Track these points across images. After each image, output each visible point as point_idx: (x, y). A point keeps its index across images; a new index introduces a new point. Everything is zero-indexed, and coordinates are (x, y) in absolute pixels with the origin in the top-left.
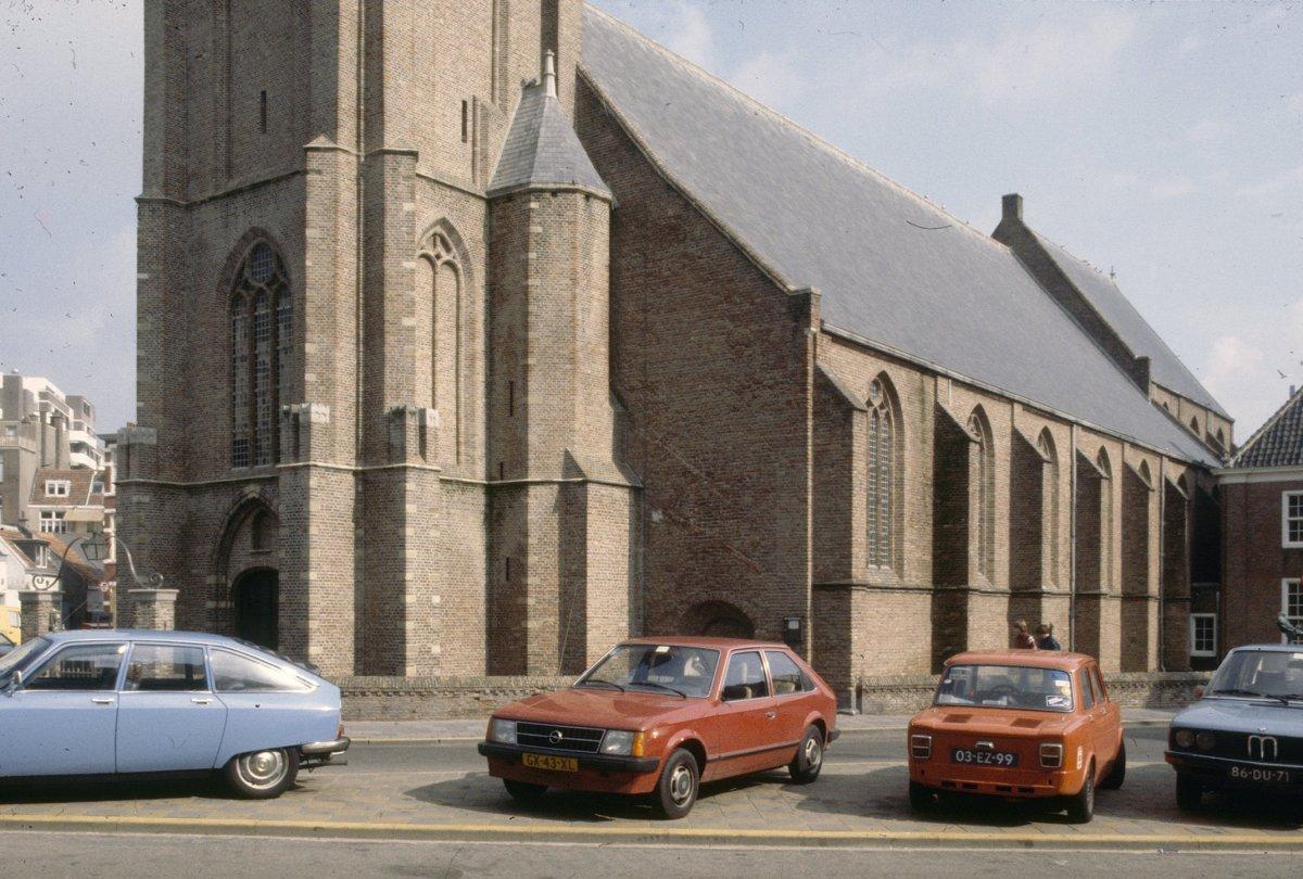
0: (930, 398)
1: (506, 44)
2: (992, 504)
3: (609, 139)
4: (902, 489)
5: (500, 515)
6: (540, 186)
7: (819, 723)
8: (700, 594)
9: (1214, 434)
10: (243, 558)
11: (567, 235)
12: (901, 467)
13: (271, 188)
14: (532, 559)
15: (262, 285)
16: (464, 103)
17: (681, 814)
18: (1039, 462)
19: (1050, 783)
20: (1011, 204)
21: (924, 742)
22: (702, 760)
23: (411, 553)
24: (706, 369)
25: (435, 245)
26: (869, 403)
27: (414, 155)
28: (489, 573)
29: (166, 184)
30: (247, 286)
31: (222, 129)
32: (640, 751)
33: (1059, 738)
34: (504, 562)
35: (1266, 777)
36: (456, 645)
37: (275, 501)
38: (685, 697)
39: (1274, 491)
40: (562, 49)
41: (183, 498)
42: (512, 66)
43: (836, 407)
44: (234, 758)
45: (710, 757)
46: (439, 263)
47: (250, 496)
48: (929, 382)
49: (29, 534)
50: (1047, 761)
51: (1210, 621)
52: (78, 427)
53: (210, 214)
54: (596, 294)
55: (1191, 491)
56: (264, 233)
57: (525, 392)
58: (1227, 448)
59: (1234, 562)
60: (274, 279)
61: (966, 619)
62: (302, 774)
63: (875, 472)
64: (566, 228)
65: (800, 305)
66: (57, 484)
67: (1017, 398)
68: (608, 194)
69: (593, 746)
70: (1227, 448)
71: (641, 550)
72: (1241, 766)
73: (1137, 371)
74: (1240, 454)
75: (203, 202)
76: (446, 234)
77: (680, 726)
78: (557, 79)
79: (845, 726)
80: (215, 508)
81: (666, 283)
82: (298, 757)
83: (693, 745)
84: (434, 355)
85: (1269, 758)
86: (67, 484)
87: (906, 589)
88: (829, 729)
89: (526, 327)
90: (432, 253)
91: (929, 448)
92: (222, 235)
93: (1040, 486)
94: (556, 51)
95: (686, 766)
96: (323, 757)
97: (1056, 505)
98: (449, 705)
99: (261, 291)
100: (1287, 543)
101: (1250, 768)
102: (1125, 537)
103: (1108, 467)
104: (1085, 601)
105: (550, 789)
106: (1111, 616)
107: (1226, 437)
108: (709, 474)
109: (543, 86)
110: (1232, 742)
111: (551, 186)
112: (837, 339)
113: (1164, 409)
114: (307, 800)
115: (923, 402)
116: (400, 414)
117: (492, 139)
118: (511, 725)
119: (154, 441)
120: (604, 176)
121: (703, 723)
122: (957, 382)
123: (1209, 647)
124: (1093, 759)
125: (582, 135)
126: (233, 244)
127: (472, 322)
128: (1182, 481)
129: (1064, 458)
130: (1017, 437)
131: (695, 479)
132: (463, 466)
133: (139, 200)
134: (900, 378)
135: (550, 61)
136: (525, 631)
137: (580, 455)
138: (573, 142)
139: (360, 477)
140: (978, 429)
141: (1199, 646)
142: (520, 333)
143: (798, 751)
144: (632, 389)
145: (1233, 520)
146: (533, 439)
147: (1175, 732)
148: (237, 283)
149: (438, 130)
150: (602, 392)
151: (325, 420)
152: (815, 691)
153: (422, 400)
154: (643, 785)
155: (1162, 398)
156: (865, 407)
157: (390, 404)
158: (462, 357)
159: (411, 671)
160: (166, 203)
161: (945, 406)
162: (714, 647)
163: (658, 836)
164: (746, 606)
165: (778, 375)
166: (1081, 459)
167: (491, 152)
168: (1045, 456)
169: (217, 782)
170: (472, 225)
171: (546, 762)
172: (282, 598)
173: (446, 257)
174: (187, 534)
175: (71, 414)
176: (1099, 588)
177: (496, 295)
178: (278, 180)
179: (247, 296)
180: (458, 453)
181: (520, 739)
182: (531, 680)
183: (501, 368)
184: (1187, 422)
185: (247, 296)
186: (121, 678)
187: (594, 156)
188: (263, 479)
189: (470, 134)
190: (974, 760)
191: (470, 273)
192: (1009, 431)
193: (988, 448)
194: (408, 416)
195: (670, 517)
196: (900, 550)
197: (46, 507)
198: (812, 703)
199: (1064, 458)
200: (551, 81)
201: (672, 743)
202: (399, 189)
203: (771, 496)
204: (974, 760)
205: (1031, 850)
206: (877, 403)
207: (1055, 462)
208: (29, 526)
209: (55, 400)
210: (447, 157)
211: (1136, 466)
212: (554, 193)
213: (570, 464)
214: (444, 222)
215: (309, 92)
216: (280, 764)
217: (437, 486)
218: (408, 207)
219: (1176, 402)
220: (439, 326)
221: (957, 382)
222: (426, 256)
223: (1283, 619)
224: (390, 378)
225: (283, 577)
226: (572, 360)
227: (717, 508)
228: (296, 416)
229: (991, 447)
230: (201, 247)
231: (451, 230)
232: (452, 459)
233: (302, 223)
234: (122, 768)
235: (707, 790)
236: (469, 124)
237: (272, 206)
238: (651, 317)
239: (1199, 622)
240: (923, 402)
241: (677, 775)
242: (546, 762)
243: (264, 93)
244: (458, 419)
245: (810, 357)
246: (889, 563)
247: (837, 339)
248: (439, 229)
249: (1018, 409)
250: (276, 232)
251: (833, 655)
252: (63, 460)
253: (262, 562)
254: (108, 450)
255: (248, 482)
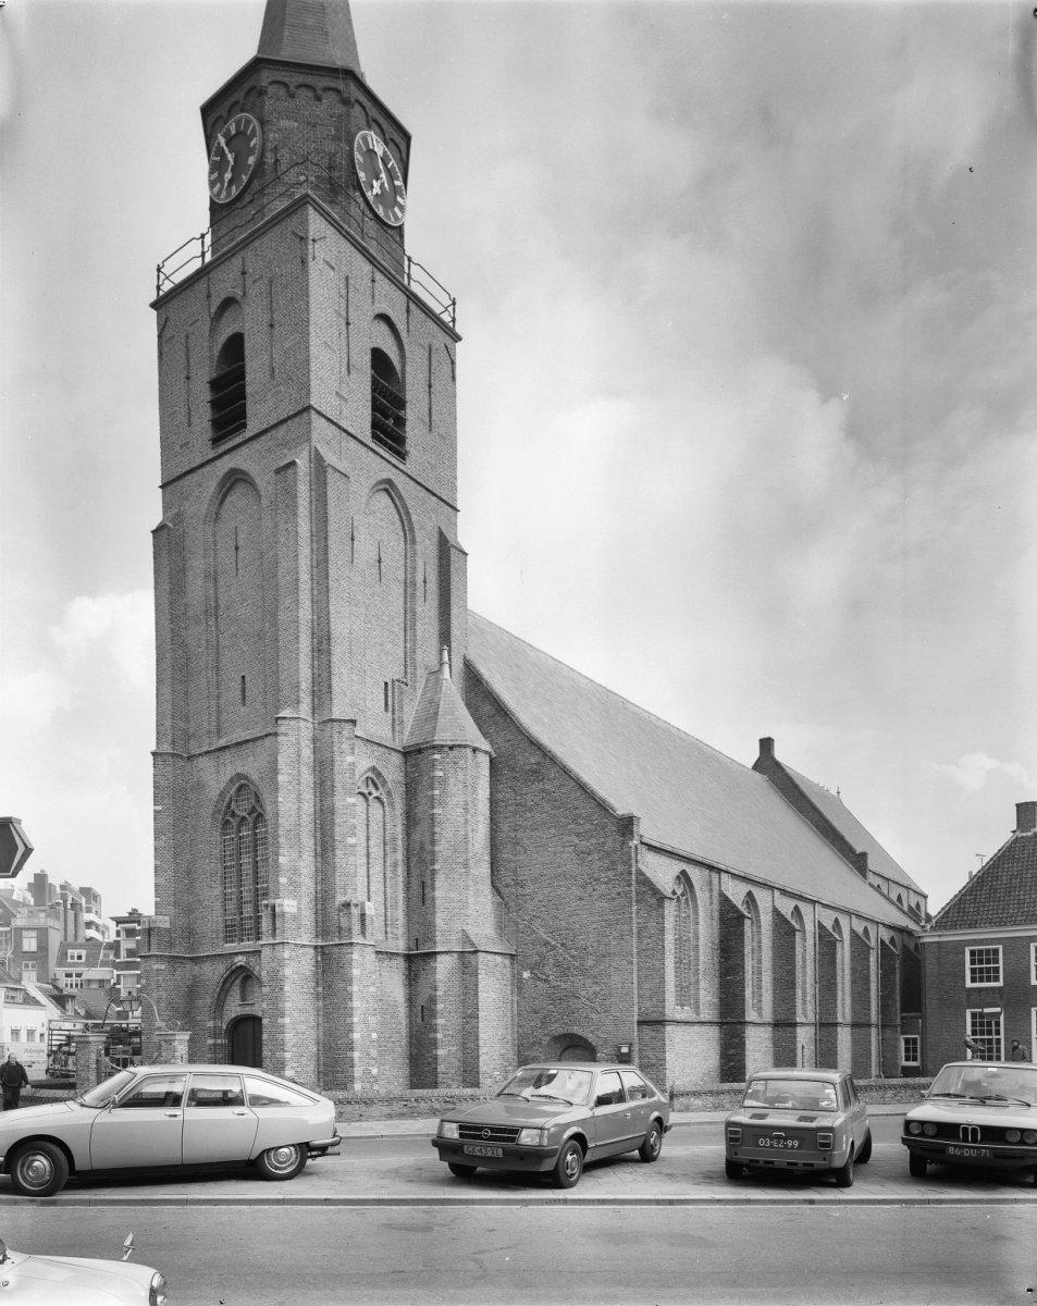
0: (716, 888)
1: (414, 642)
2: (760, 962)
3: (487, 708)
4: (698, 952)
5: (416, 975)
6: (441, 743)
7: (659, 1120)
8: (557, 1029)
9: (913, 906)
10: (234, 1009)
11: (461, 778)
12: (697, 938)
13: (250, 745)
14: (440, 1006)
15: (245, 814)
16: (386, 683)
17: (572, 1185)
18: (792, 931)
19: (825, 1160)
20: (766, 744)
21: (736, 1132)
22: (585, 1148)
23: (356, 1004)
24: (559, 870)
25: (367, 786)
26: (674, 893)
27: (354, 722)
28: (410, 1017)
29: (173, 742)
30: (233, 814)
31: (213, 702)
32: (545, 1142)
33: (831, 1129)
34: (420, 1008)
35: (974, 1153)
36: (387, 1067)
37: (257, 968)
38: (1029, 1106)
39: (958, 948)
40: (453, 645)
41: (189, 966)
42: (419, 656)
43: (652, 896)
44: (264, 1151)
45: (590, 1145)
46: (371, 798)
47: (239, 964)
48: (715, 876)
49: (61, 991)
50: (822, 1145)
51: (915, 1040)
52: (89, 910)
53: (204, 762)
54: (481, 818)
55: (899, 948)
56: (246, 778)
57: (434, 889)
58: (923, 916)
59: (931, 1001)
60: (253, 809)
61: (744, 1043)
62: (309, 1162)
63: (679, 941)
64: (460, 773)
65: (627, 825)
66: (76, 952)
67: (777, 886)
68: (485, 745)
69: (513, 1140)
70: (923, 916)
71: (515, 999)
72: (955, 1146)
73: (858, 862)
74: (934, 921)
75: (200, 755)
76: (375, 778)
77: (569, 1125)
78: (450, 665)
79: (386, 1126)
80: (213, 973)
81: (530, 810)
82: (306, 1150)
83: (578, 1137)
84: (368, 863)
85: (974, 1141)
86: (84, 953)
87: (702, 1023)
88: (665, 1124)
89: (433, 843)
90: (366, 792)
91: (716, 923)
92: (215, 778)
93: (794, 948)
94: (449, 646)
95: (575, 1152)
96: (323, 1150)
97: (804, 961)
98: (387, 1110)
99: (244, 818)
100: (969, 984)
101: (961, 1147)
102: (853, 982)
103: (840, 933)
104: (826, 1026)
105: (479, 1169)
106: (844, 1037)
107: (922, 908)
108: (563, 945)
109: (440, 670)
110: (948, 1130)
111: (448, 743)
112: (651, 848)
113: (878, 889)
114: (314, 1180)
115: (711, 890)
116: (347, 905)
117: (406, 710)
118: (455, 1126)
119: (168, 926)
120: (485, 735)
121: (582, 1122)
122: (734, 876)
123: (915, 1059)
124: (853, 1143)
125: (469, 705)
126: (222, 785)
127: (394, 839)
128: (892, 940)
129: (809, 927)
130: (776, 912)
131: (554, 948)
132: (390, 940)
133: (154, 754)
134: (695, 874)
135: (446, 653)
136: (436, 1058)
137: (472, 932)
138: (463, 711)
139: (319, 950)
140: (748, 908)
141: (907, 1059)
142: (428, 847)
143: (645, 1141)
144: (507, 886)
145: (930, 967)
146: (439, 921)
147: (729, 1124)
148: (226, 813)
149: (369, 705)
150: (487, 888)
151: (295, 910)
152: (655, 1099)
153: (359, 896)
154: (548, 1165)
155: (877, 881)
156: (671, 896)
157: (340, 899)
158: (388, 864)
159: (358, 1087)
160: (173, 755)
161: (727, 893)
162: (590, 1069)
163: (559, 1200)
164: (591, 1038)
165: (610, 874)
166: (821, 927)
167: (405, 719)
168: (797, 927)
169: (252, 1169)
170: (393, 770)
171: (480, 1151)
172: (265, 1037)
173: (375, 794)
174: (192, 991)
175: (83, 901)
176: (836, 1018)
177: (411, 821)
178: (255, 740)
179: (234, 822)
180: (386, 932)
181: (461, 1135)
182: (441, 1091)
183: (415, 872)
184: (894, 897)
185: (234, 822)
186: (185, 1100)
187: (478, 720)
188: (249, 952)
189: (390, 706)
190: (772, 1145)
191: (392, 804)
192: (770, 909)
193: (757, 922)
194: (353, 907)
195: (536, 975)
196: (697, 994)
197: (69, 970)
198: (652, 1107)
199: (809, 927)
200: (446, 668)
201: (565, 1136)
202: (344, 746)
203: (607, 960)
204: (772, 1145)
205: (813, 1206)
206: (679, 892)
207: (803, 931)
208: (61, 984)
209: (72, 891)
210: (376, 724)
211: (860, 931)
212: (451, 748)
213: (466, 938)
214: (374, 769)
215: (278, 678)
216: (294, 1156)
217: (373, 956)
218: (350, 759)
219: (886, 884)
220: (371, 843)
221: (734, 876)
222: (360, 793)
223: (968, 1039)
224: (339, 881)
225: (265, 1021)
226: (466, 865)
227: (569, 968)
228: (274, 907)
229: (759, 921)
230: (199, 786)
231: (379, 775)
232: (381, 936)
233: (275, 771)
234: (96, 1166)
235: (589, 1167)
236: (390, 699)
237: (251, 758)
238: (519, 835)
239: (907, 1041)
240: (711, 890)
241: (569, 1158)
242: (480, 1151)
243: (243, 677)
244: (386, 908)
245: (633, 862)
246: (689, 1005)
247: (651, 848)
248: (370, 774)
249: (777, 893)
250: (254, 776)
251: (653, 1067)
252: (80, 934)
253: (248, 1010)
254: (119, 928)
255: (236, 954)
